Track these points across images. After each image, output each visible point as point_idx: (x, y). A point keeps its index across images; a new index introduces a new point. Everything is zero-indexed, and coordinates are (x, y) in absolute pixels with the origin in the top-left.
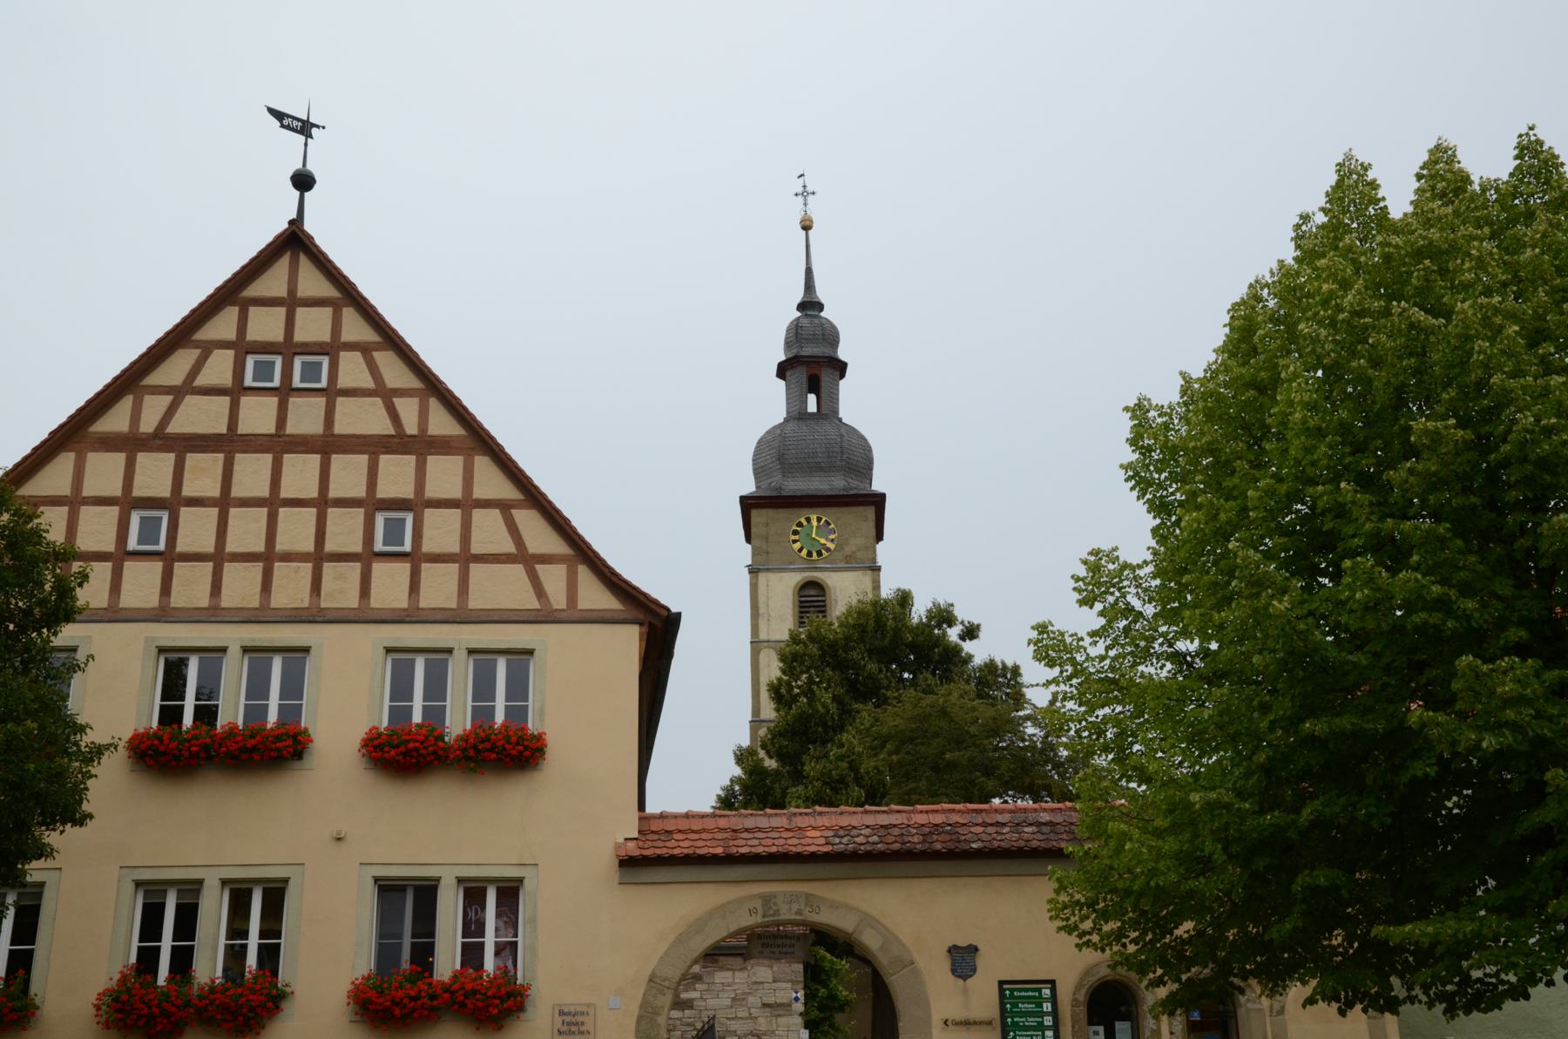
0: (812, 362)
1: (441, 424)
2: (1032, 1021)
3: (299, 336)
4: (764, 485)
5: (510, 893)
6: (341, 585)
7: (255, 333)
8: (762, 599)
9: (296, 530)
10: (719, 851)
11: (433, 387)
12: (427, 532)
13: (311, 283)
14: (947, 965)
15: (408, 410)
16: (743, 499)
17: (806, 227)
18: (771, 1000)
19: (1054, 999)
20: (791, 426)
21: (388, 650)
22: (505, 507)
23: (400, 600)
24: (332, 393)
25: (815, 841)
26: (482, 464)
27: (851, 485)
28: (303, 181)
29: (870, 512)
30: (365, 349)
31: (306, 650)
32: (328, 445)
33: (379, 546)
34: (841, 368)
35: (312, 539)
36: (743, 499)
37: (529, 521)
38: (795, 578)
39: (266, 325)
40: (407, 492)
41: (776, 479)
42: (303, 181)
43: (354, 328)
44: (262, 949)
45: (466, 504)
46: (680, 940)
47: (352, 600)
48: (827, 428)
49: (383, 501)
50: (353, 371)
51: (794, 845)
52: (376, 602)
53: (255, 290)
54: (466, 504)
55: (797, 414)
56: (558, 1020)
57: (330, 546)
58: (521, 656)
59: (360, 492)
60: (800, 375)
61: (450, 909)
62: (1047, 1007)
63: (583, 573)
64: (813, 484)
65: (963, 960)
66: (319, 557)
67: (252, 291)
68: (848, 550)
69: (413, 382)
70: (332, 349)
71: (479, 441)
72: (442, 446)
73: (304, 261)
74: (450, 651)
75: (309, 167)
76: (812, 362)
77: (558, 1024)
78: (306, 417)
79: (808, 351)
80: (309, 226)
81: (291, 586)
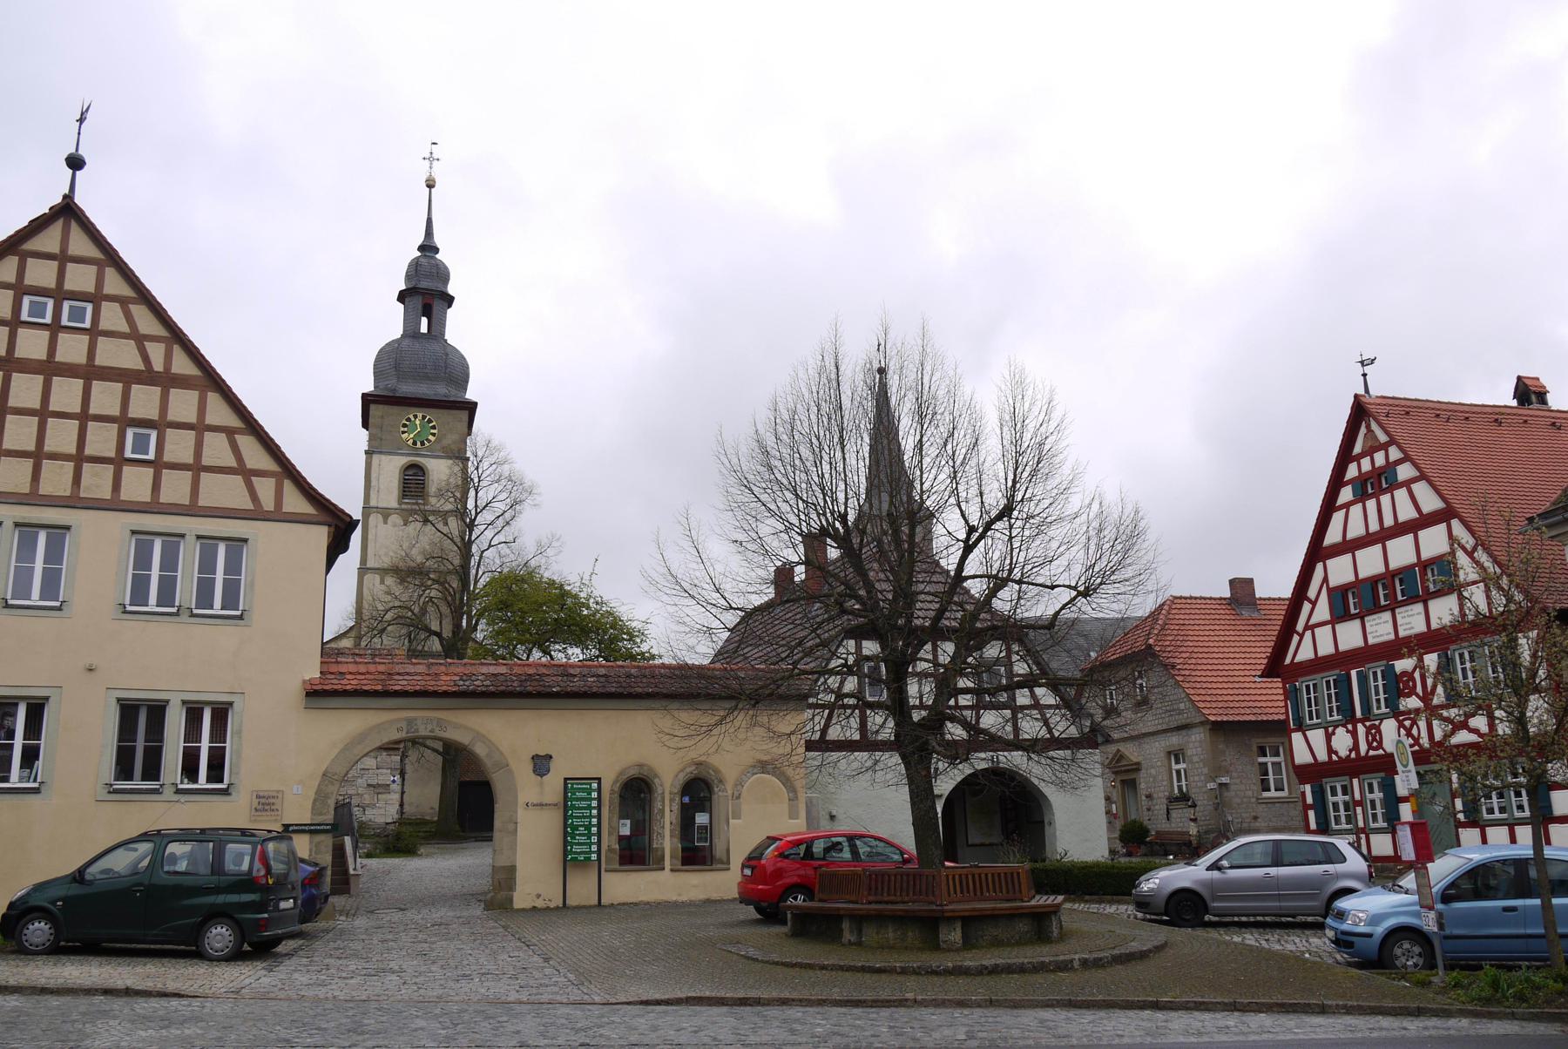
0: (426, 292)
1: (182, 365)
2: (584, 804)
3: (68, 286)
4: (382, 385)
5: (221, 714)
6: (97, 481)
7: (30, 279)
8: (374, 475)
9: (62, 436)
10: (379, 688)
11: (177, 337)
12: (168, 447)
13: (80, 244)
14: (531, 767)
15: (156, 353)
16: (364, 395)
17: (430, 185)
18: (374, 782)
19: (599, 790)
20: (406, 342)
21: (134, 532)
22: (230, 432)
23: (145, 495)
24: (94, 332)
25: (445, 683)
26: (213, 398)
27: (453, 395)
28: (75, 163)
29: (465, 415)
30: (123, 302)
31: (68, 528)
32: (90, 373)
33: (128, 454)
34: (449, 300)
35: (75, 444)
36: (364, 395)
37: (247, 443)
38: (402, 461)
39: (41, 274)
40: (153, 414)
41: (392, 383)
42: (75, 163)
43: (114, 284)
44: (25, 748)
45: (200, 428)
46: (346, 748)
47: (106, 494)
48: (435, 346)
49: (133, 420)
50: (112, 317)
51: (431, 685)
52: (125, 495)
53: (33, 245)
54: (200, 428)
55: (411, 332)
56: (256, 801)
57: (89, 450)
58: (237, 544)
59: (115, 411)
60: (418, 302)
61: (175, 723)
62: (594, 795)
63: (288, 486)
64: (419, 390)
65: (541, 764)
66: (80, 458)
67: (30, 245)
68: (445, 442)
69: (160, 331)
70: (96, 298)
71: (212, 381)
72: (183, 382)
73: (74, 226)
74: (183, 536)
75: (80, 152)
76: (426, 292)
77: (255, 804)
78: (72, 349)
79: (424, 284)
80: (79, 200)
81: (56, 479)
